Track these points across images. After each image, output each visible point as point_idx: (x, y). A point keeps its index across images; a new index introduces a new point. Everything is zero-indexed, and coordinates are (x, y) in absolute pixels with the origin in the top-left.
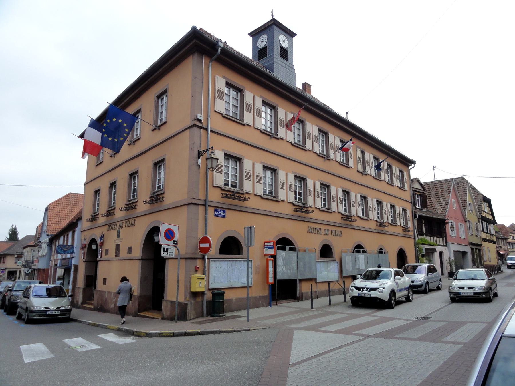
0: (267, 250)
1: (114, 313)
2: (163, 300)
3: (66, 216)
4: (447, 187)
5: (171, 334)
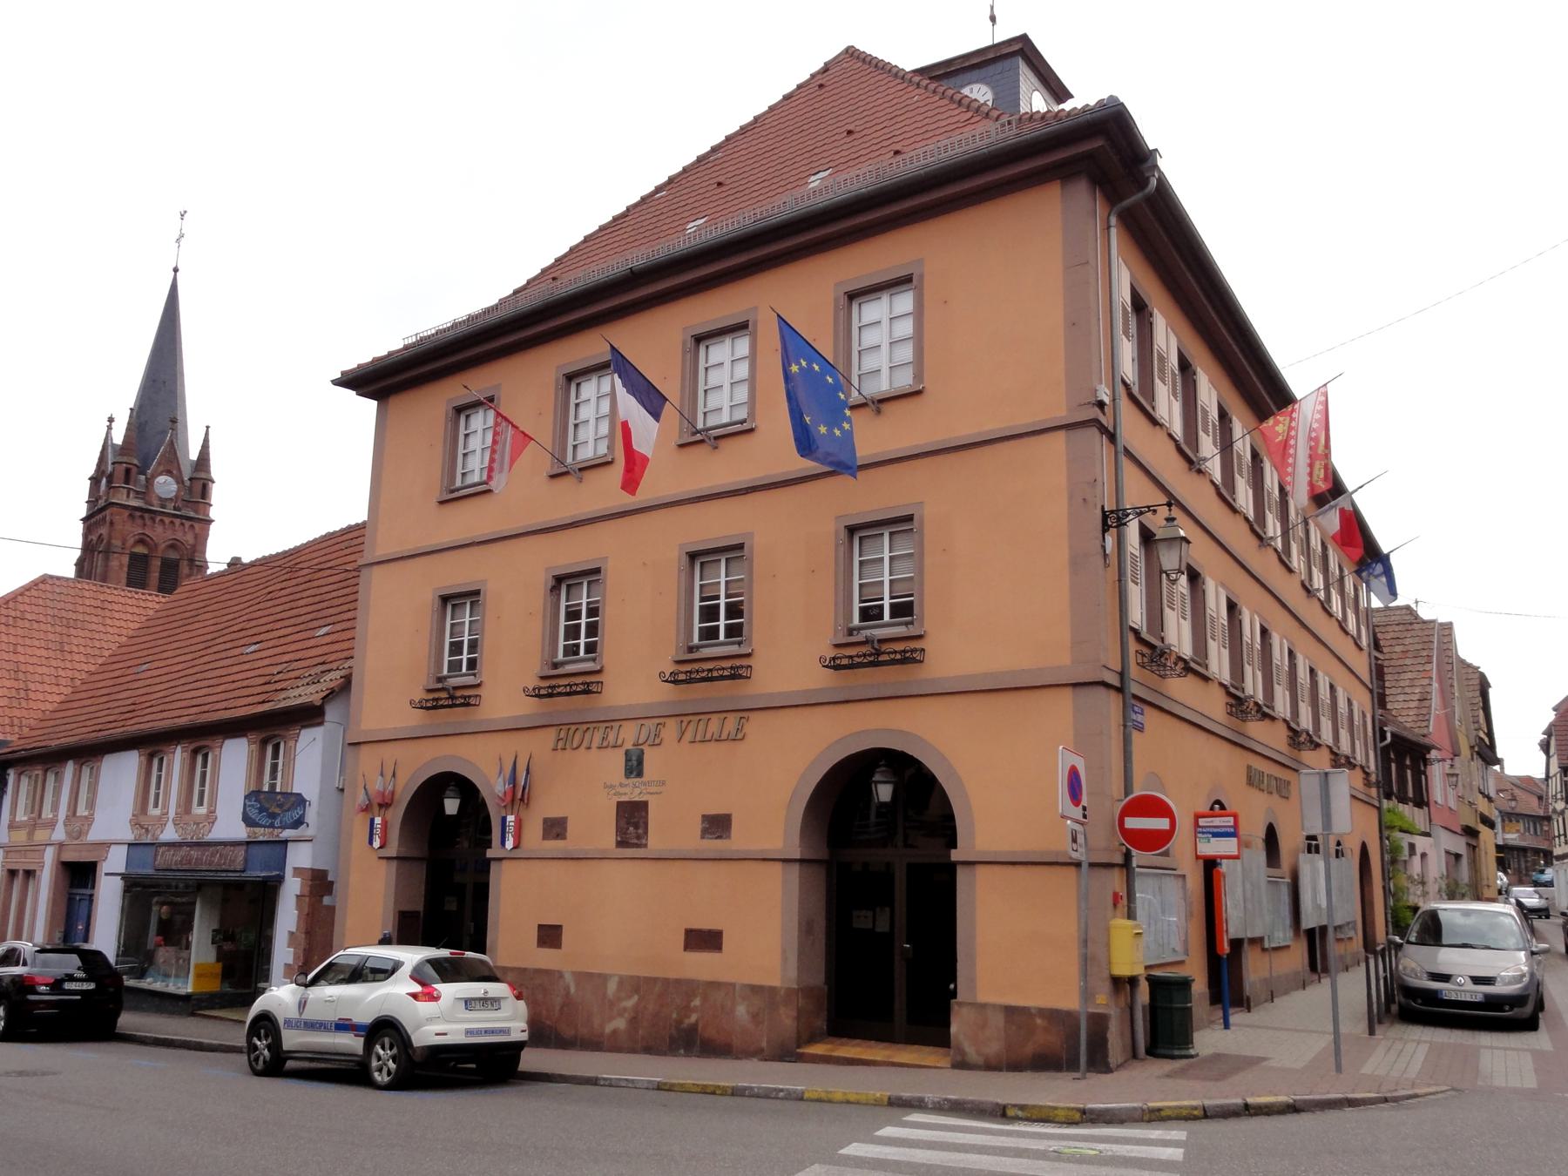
0: (1209, 841)
1: (633, 1051)
2: (957, 1003)
3: (45, 670)
4: (1417, 640)
5: (1196, 1113)
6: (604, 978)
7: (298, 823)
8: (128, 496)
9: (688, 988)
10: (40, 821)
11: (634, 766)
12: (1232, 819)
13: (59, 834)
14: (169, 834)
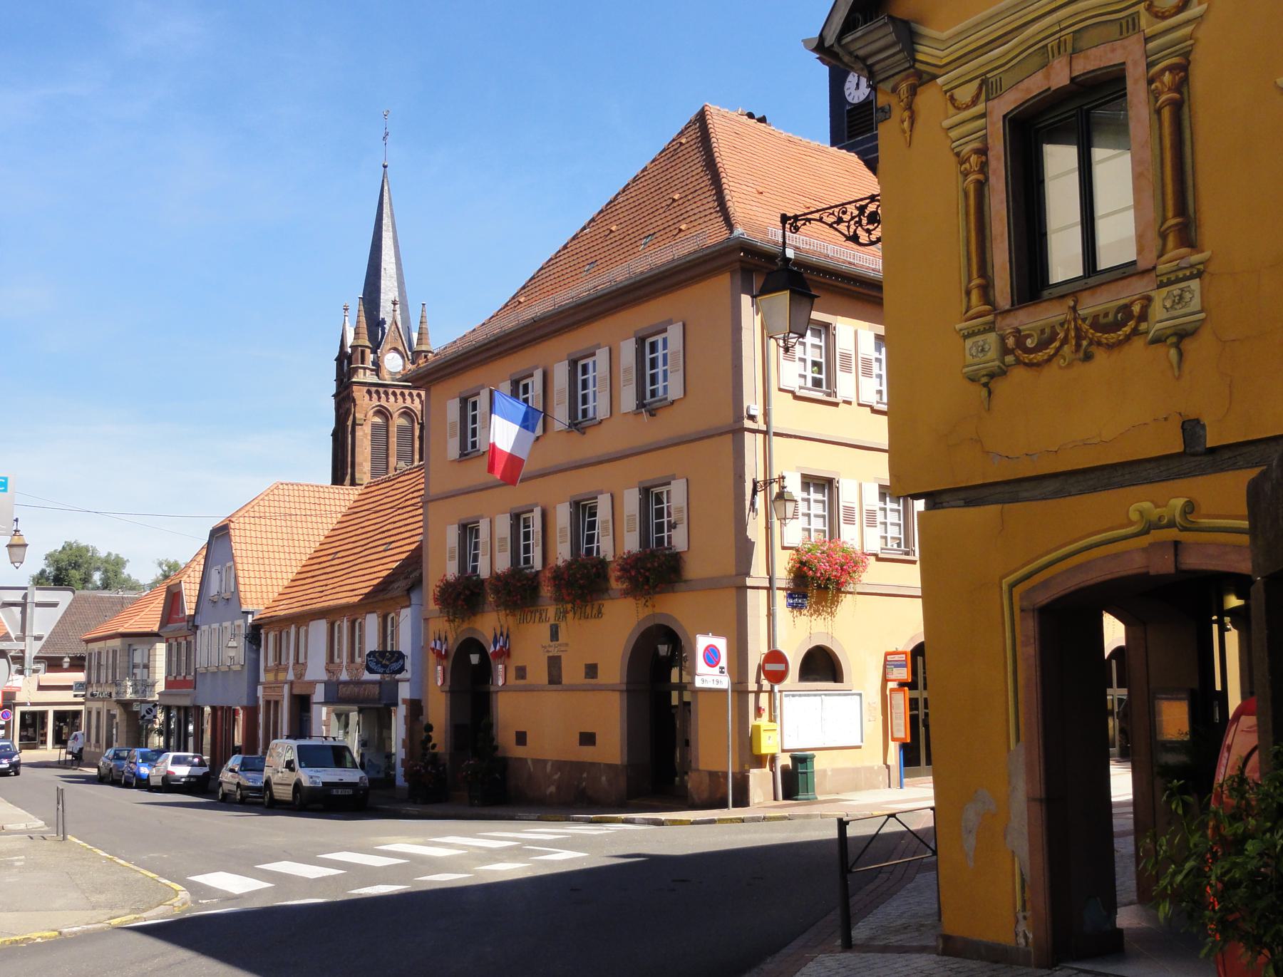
6: (545, 762)
7: (402, 669)
8: (365, 374)
9: (580, 766)
10: (280, 667)
11: (554, 635)
12: (904, 656)
13: (291, 676)
14: (344, 676)
